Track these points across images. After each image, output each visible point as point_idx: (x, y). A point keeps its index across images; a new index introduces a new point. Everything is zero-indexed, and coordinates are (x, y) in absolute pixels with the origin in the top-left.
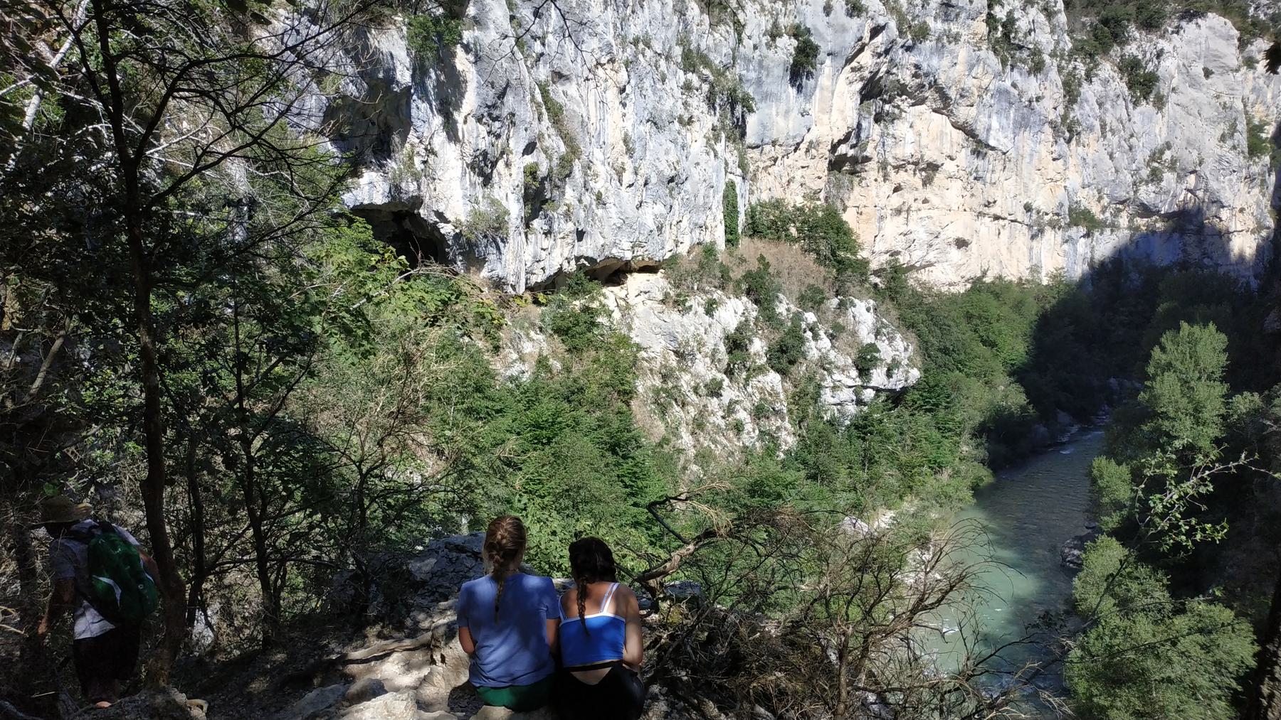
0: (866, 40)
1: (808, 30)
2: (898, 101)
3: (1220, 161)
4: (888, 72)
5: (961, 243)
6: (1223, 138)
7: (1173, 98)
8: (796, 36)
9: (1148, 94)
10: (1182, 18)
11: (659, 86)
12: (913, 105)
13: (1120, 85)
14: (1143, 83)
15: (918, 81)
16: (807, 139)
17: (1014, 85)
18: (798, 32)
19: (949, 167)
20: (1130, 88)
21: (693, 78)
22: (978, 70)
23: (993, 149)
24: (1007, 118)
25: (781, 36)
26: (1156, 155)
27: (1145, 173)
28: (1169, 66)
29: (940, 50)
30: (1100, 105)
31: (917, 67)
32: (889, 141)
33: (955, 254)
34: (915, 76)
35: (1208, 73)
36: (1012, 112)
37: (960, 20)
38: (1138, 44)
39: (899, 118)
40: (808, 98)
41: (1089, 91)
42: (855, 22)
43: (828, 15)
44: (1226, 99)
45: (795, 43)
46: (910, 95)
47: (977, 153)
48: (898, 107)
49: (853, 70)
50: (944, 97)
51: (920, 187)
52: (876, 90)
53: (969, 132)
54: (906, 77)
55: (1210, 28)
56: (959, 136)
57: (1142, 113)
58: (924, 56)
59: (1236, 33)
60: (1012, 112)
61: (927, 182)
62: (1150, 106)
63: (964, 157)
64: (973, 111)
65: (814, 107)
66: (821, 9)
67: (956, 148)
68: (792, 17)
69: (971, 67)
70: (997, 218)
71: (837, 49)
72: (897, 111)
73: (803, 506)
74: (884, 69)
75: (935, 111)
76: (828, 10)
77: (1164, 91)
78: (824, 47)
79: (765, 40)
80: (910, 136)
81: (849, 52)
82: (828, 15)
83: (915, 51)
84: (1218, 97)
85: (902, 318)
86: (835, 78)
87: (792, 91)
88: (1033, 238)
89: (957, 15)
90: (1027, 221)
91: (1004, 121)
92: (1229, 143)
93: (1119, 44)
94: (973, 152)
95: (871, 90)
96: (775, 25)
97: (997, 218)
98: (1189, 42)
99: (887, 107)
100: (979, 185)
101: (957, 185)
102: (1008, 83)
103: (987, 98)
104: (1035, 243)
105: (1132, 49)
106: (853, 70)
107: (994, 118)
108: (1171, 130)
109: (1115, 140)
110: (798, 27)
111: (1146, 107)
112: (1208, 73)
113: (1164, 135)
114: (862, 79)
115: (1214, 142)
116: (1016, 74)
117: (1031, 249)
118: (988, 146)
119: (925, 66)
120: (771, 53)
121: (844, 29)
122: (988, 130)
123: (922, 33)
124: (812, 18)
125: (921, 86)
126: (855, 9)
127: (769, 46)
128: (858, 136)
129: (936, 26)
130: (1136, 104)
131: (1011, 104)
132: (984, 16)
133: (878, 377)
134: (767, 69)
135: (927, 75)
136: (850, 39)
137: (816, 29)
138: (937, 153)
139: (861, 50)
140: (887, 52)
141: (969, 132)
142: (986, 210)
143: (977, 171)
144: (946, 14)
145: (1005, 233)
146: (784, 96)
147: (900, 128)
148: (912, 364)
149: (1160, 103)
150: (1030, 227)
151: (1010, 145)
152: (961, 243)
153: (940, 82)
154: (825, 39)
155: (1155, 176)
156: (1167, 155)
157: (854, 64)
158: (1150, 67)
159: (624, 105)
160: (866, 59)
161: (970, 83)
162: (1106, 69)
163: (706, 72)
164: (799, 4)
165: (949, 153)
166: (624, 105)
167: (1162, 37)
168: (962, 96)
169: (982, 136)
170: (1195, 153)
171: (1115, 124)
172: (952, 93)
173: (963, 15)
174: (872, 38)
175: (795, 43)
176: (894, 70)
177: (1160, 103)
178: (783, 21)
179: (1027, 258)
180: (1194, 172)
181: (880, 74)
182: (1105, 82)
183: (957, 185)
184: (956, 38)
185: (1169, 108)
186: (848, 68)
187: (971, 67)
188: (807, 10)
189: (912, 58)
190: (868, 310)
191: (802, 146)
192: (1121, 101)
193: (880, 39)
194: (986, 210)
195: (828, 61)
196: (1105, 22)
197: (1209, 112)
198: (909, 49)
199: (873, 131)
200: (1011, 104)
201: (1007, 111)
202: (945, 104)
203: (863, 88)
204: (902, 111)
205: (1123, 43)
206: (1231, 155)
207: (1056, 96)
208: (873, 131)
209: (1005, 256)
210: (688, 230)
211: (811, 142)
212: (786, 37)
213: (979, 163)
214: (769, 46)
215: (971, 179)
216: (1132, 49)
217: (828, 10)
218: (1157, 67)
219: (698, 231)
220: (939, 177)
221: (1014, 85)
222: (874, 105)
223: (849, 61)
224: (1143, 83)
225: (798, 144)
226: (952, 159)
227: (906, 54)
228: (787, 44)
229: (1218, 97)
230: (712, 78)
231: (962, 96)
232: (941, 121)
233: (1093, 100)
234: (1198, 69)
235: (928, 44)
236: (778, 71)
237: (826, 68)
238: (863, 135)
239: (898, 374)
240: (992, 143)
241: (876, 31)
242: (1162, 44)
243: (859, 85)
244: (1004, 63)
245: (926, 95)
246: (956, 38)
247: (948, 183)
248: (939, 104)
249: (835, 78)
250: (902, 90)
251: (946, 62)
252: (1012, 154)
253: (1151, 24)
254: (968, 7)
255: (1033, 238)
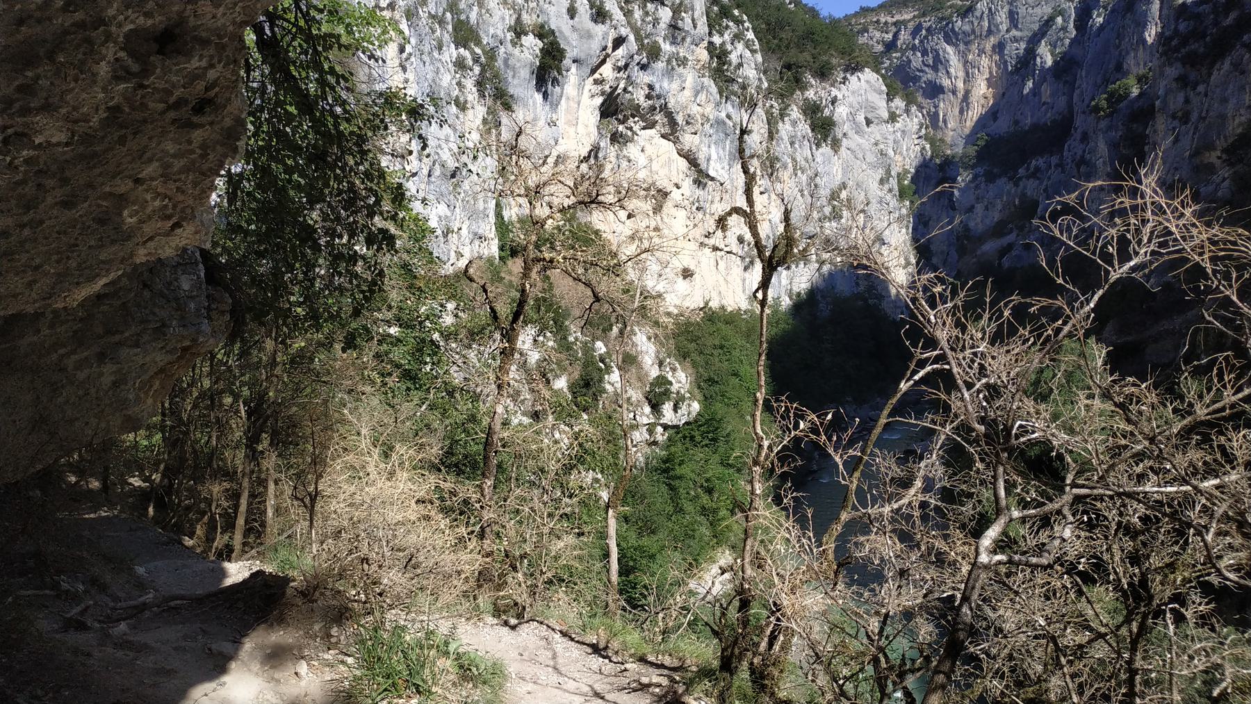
0: (609, 51)
1: (553, 32)
2: (631, 122)
3: (880, 202)
4: (625, 89)
5: (687, 274)
6: (882, 182)
7: (845, 142)
8: (540, 36)
9: (827, 136)
10: (846, 71)
11: (436, 54)
12: (644, 128)
13: (804, 128)
14: (823, 128)
15: (650, 102)
16: (554, 154)
17: (729, 117)
18: (542, 32)
19: (676, 195)
20: (813, 130)
21: (466, 53)
22: (702, 97)
23: (713, 179)
24: (724, 149)
25: (526, 34)
26: (834, 196)
27: (827, 210)
28: (841, 112)
29: (669, 72)
30: (792, 144)
31: (651, 87)
32: (624, 164)
33: (682, 285)
34: (648, 97)
35: (868, 122)
36: (728, 142)
37: (686, 45)
38: (815, 91)
39: (632, 140)
40: (555, 106)
41: (785, 129)
42: (599, 29)
43: (572, 18)
44: (882, 146)
45: (540, 44)
46: (643, 118)
47: (698, 183)
48: (631, 129)
49: (596, 82)
50: (673, 123)
51: (651, 213)
52: (613, 108)
53: (692, 161)
54: (639, 96)
55: (867, 82)
56: (683, 164)
57: (823, 154)
58: (655, 76)
59: (884, 88)
60: (728, 142)
61: (658, 209)
62: (829, 149)
63: (687, 185)
64: (697, 138)
65: (562, 114)
66: (565, 11)
67: (682, 176)
68: (534, 17)
69: (697, 94)
70: (715, 249)
71: (582, 56)
72: (629, 133)
73: (1219, 661)
74: (622, 85)
75: (663, 136)
76: (572, 12)
77: (840, 136)
78: (571, 54)
79: (510, 35)
80: (642, 160)
81: (595, 61)
82: (572, 18)
83: (649, 71)
84: (876, 144)
85: (678, 348)
86: (581, 86)
87: (538, 97)
88: (746, 269)
89: (683, 39)
90: (740, 253)
91: (721, 152)
92: (886, 187)
93: (800, 89)
94: (695, 182)
95: (611, 108)
96: (518, 20)
97: (715, 249)
98: (853, 93)
99: (621, 128)
100: (700, 215)
101: (682, 214)
102: (723, 115)
103: (707, 126)
104: (747, 275)
105: (810, 94)
106: (596, 82)
107: (713, 146)
108: (845, 172)
109: (804, 178)
110: (542, 26)
111: (826, 149)
112: (868, 122)
113: (840, 177)
114: (603, 93)
115: (876, 185)
116: (729, 106)
117: (744, 280)
118: (708, 176)
119: (657, 86)
120: (517, 51)
121: (589, 36)
122: (708, 160)
123: (654, 53)
124: (558, 20)
125: (653, 108)
126: (600, 15)
127: (514, 44)
128: (596, 157)
129: (666, 47)
130: (818, 146)
131: (727, 135)
132: (705, 44)
133: (668, 415)
134: (514, 69)
135: (659, 97)
136: (595, 46)
137: (561, 32)
138: (666, 181)
139: (603, 62)
140: (626, 66)
141: (692, 161)
142: (706, 241)
143: (698, 201)
144: (674, 38)
145: (722, 265)
146: (531, 101)
147: (632, 150)
148: (692, 398)
149: (836, 145)
150: (742, 258)
151: (727, 176)
152: (687, 274)
153: (670, 105)
154: (573, 46)
155: (836, 215)
156: (844, 195)
157: (597, 76)
158: (827, 112)
159: (404, 69)
160: (607, 71)
161: (695, 109)
162: (795, 112)
163: (478, 51)
164: (541, 2)
165: (676, 181)
166: (404, 69)
167: (832, 85)
168: (688, 123)
169: (703, 166)
170: (863, 194)
171: (803, 163)
172: (680, 119)
173: (688, 40)
174: (614, 50)
175: (540, 44)
176: (630, 89)
177: (836, 145)
178: (528, 19)
179: (741, 288)
180: (863, 211)
181: (619, 91)
182: (794, 123)
183: (682, 214)
184: (683, 62)
185: (843, 150)
186: (591, 79)
187: (697, 94)
188: (552, 10)
189: (644, 78)
190: (649, 338)
191: (549, 160)
192: (806, 142)
193: (620, 52)
194: (706, 241)
195: (574, 69)
196: (788, 67)
197: (871, 158)
198: (643, 67)
199: (610, 152)
200: (727, 135)
201: (724, 142)
202: (672, 132)
203: (602, 104)
204: (634, 133)
205: (804, 88)
206: (889, 197)
207: (762, 131)
208: (610, 152)
209: (723, 288)
210: (468, 241)
211: (558, 157)
212: (531, 36)
213: (699, 192)
214: (514, 44)
215: (694, 208)
216: (810, 94)
217: (572, 12)
218: (832, 112)
219: (477, 242)
220: (668, 207)
221: (729, 117)
222: (613, 124)
223: (593, 71)
224: (823, 128)
225: (547, 157)
226: (678, 188)
227: (641, 73)
228: (531, 43)
229: (876, 144)
230: (483, 59)
231: (688, 123)
232: (667, 146)
233: (786, 138)
234: (861, 118)
235: (660, 65)
236: (525, 73)
237: (573, 76)
238: (600, 155)
239: (684, 409)
240: (712, 173)
241: (619, 42)
242: (834, 92)
243: (600, 100)
244: (721, 93)
245: (657, 118)
246: (683, 62)
247: (674, 211)
248: (667, 130)
249: (581, 86)
250: (636, 111)
251: (675, 86)
252: (728, 185)
253: (823, 73)
254: (692, 32)
255: (746, 269)
